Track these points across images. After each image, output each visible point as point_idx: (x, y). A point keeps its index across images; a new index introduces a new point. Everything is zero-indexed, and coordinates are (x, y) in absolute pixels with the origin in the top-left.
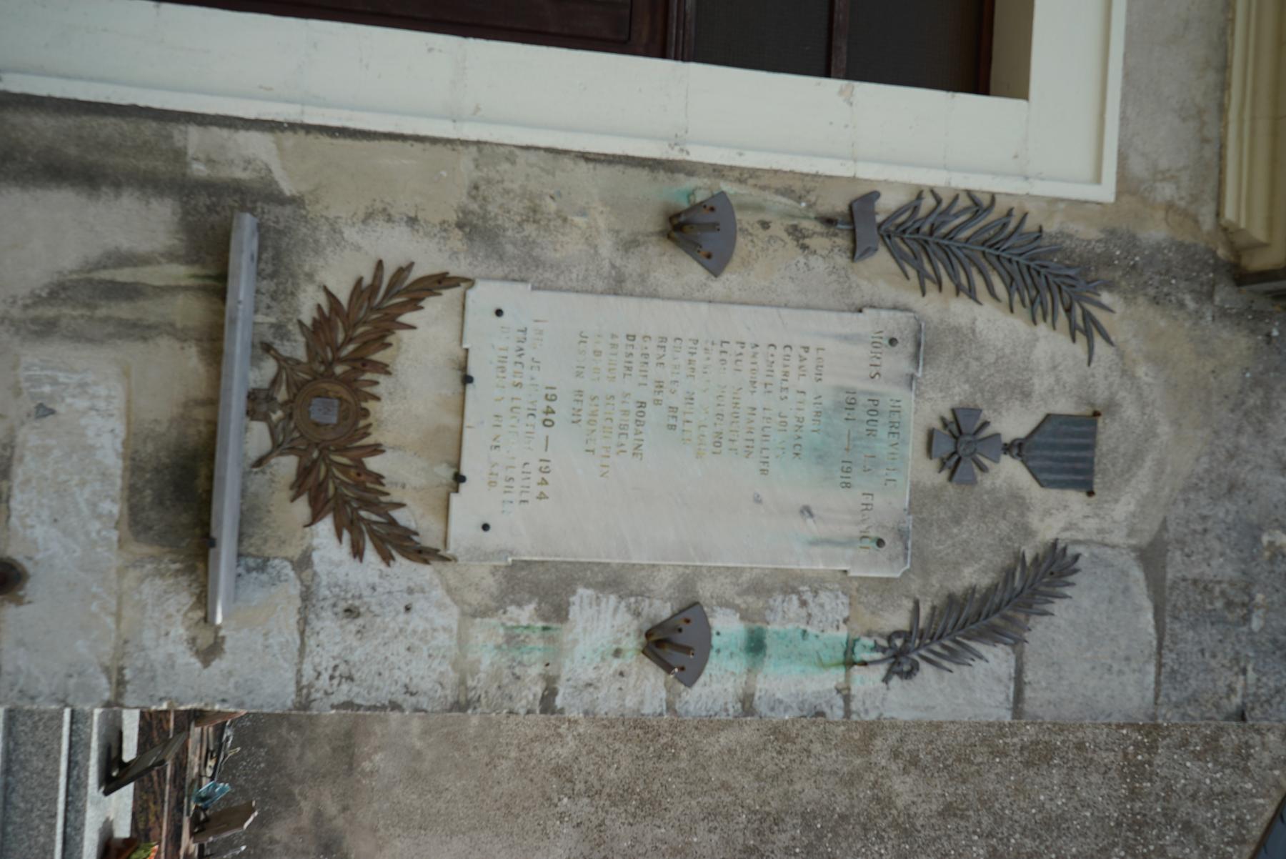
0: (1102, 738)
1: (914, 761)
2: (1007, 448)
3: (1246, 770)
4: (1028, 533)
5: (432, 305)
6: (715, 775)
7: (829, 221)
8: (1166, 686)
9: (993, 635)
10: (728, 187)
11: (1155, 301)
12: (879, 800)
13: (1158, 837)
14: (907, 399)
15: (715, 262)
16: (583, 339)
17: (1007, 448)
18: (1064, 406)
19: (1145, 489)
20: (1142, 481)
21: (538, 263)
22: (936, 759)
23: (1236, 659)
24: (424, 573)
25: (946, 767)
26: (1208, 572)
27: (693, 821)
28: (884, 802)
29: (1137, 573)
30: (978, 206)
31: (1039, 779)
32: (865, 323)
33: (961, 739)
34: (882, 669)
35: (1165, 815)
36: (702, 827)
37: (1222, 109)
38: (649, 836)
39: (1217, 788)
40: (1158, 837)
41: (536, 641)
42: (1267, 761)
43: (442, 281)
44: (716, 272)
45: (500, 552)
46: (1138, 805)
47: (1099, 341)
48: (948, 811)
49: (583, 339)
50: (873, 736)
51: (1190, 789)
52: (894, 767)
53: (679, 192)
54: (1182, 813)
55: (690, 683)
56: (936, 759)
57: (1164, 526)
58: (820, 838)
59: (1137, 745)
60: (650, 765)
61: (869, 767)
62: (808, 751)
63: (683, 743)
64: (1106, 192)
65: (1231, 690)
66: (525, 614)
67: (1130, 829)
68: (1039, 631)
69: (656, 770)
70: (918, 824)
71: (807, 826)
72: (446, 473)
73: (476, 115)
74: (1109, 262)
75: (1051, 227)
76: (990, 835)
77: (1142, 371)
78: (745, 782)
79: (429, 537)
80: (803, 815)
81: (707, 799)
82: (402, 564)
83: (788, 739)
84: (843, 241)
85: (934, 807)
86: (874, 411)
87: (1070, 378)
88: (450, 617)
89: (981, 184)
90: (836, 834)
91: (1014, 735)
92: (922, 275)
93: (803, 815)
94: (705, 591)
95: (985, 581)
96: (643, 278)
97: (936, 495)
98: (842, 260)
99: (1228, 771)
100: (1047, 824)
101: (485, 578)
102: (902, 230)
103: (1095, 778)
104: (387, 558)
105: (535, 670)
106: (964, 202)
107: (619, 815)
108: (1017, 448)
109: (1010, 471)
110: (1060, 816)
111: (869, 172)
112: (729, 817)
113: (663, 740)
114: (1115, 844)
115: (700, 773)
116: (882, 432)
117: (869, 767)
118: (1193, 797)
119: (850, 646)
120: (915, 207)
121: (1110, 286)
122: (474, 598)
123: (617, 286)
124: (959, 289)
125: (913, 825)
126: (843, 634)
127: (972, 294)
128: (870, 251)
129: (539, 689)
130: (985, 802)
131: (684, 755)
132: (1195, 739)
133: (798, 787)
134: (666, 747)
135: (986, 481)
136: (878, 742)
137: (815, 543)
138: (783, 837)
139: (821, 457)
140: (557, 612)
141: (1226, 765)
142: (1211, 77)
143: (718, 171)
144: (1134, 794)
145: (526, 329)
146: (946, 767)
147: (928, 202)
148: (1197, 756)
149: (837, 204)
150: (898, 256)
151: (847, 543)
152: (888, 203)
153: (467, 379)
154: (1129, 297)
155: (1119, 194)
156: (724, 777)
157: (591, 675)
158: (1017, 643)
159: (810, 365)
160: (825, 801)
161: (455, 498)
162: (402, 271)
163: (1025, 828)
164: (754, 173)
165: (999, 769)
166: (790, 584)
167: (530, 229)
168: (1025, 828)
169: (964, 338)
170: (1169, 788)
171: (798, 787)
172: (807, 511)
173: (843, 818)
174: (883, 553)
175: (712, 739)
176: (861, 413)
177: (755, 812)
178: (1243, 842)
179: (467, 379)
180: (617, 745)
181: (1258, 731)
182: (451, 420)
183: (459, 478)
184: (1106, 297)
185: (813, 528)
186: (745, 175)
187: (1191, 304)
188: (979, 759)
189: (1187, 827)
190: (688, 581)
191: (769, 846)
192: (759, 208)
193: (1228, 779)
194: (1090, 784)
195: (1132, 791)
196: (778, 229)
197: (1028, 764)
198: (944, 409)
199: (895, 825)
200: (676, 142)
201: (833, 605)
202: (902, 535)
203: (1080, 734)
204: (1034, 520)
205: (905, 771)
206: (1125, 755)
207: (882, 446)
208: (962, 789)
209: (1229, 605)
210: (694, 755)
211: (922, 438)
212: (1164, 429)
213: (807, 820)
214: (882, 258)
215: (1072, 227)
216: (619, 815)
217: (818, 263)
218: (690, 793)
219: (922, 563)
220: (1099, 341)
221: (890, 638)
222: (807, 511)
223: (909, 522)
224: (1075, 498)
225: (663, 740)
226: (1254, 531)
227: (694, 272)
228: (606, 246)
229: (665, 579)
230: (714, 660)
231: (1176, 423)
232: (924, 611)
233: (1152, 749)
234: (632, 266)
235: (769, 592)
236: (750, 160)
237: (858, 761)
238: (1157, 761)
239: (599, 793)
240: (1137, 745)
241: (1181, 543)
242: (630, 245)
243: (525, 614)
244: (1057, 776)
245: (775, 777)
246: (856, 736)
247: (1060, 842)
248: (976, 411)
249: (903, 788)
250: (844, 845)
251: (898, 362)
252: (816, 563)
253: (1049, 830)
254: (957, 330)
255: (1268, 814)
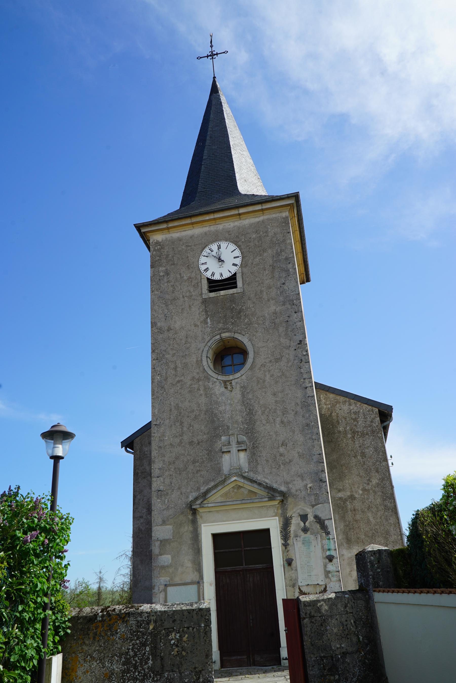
0: (358, 443)
1: (369, 480)
2: (305, 525)
3: (359, 412)
4: (313, 521)
5: (302, 589)
6: (379, 520)
7: (286, 548)
8: (326, 502)
9: (324, 523)
10: (285, 560)
11: (287, 510)
12: (378, 486)
13: (375, 427)
14: (302, 537)
15: (292, 560)
16: (302, 573)
17: (305, 525)
18: (299, 519)
19: (306, 508)
20: (305, 508)
21: (296, 579)
22: (368, 476)
23: (322, 494)
24: (328, 586)
25: (369, 473)
26: (314, 499)
27: (389, 523)
28: (378, 485)
29: (315, 507)
30: (281, 532)
31: (368, 454)
32: (295, 543)
33: (363, 471)
34: (329, 535)
35: (370, 427)
36: (390, 521)
37: (266, 506)
38: (393, 532)
39: (363, 417)
40: (375, 427)
41: (332, 574)
42: (356, 408)
43: (299, 589)
44: (293, 560)
45: (324, 578)
46: (369, 433)
47: (292, 516)
48: (377, 471)
49: (302, 573)
50: (366, 489)
51: (364, 422)
52: (371, 484)
53: (286, 565)
54: (369, 423)
55: (334, 556)
56: (368, 476)
57: (310, 505)
58: (387, 497)
59: (358, 435)
60: (379, 534)
61: (372, 489)
62: (371, 502)
63: (374, 528)
64: (277, 518)
65: (325, 494)
66: (330, 575)
67: (374, 433)
68: (323, 518)
69: (380, 532)
70: (381, 477)
71: (385, 500)
72: (318, 586)
73: (283, 587)
74: (284, 516)
75: (282, 523)
76: (380, 462)
77: (294, 510)
78: (379, 514)
79: (324, 586)
80: (383, 501)
81: (384, 521)
82: (327, 589)
83: (369, 506)
84: (288, 546)
85: (377, 474)
86: (304, 540)
87: (297, 518)
88: (331, 583)
89: (279, 532)
90: (386, 493)
91: (360, 461)
92: (289, 537)
93: (383, 501)
94: (325, 556)
95: (319, 525)
96: (295, 567)
97: (311, 532)
98: (289, 546)
99: (359, 416)
100: (376, 451)
101: (327, 580)
102: (285, 540)
103: (366, 442)
104: (327, 590)
105: (335, 573)
106: (281, 533)
107: (390, 539)
108: (305, 523)
109: (307, 524)
110: (374, 448)
111: (280, 545)
112: (387, 516)
113: (374, 532)
114: (378, 436)
115: (379, 523)
116: (305, 539)
117: (372, 489)
118: (366, 422)
119: (328, 539)
120: (283, 539)
121: (286, 515)
122: (329, 581)
123: (296, 570)
124: (290, 533)
125: (381, 478)
126: (327, 540)
127: (290, 531)
128: (288, 543)
129: (337, 573)
130: (374, 464)
131: (376, 527)
132: (354, 423)
133: (378, 503)
134: (375, 531)
135: (309, 527)
136: (367, 488)
137: (318, 545)
138: (388, 504)
139: (309, 546)
140: (329, 572)
141: (358, 416)
142: (263, 507)
143: (283, 561)
144: (367, 434)
145: (138, 227)
146: (369, 473)
147: (282, 537)
148: (358, 422)
149: (284, 547)
150: (288, 540)
151: (317, 541)
152: (283, 542)
153: (308, 585)
154: (287, 513)
155: (277, 516)
156: (379, 518)
157: (335, 567)
158: (324, 520)
159: (300, 548)
160: (380, 497)
161: (320, 584)
162: (299, 593)
163: (378, 455)
164: (283, 557)
165: (367, 462)
166: (323, 547)
167: (293, 580)
168: (378, 455)
169: (295, 531)
170: (365, 427)
171: (378, 503)
172: (315, 546)
173: (382, 493)
174: (318, 537)
175: (372, 522)
176: (304, 542)
177: (385, 511)
178: (372, 410)
179: (308, 585)
180: (377, 541)
181: (351, 411)
182: (313, 586)
183: (318, 584)
184: (288, 516)
185: (316, 545)
186: (283, 558)
187: (287, 506)
188: (366, 467)
189: (372, 422)
190: (324, 558)
191: (391, 507)
192: (286, 556)
193: (361, 415)
194: (367, 443)
195: (367, 434)
196: (288, 554)
197: (365, 457)
198: (302, 532)
199: (382, 482)
200: (281, 566)
201: (324, 542)
202: (315, 535)
203: (358, 447)
204: (312, 520)
205: (371, 481)
206: (360, 437)
207: (307, 539)
208: (373, 469)
209: (316, 496)
210: (376, 525)
211: (305, 534)
212: (300, 507)
213: (384, 500)
214: (288, 542)
215: (281, 521)
216: (390, 539)
217: (290, 549)
218: (383, 525)
219: (318, 533)
220: (292, 516)
221: (326, 535)
222: (315, 546)
223: (314, 535)
224: (309, 516)
225: (374, 532)
226: (309, 494)
227: (293, 562)
228: (293, 572)
229: (324, 561)
230: (331, 554)
231: (299, 505)
232: (323, 531)
233: (358, 432)
234: (294, 569)
235: (324, 549)
236: (282, 558)
237: (371, 491)
238: (360, 430)
239: (387, 543)
240: (358, 435)
241: (311, 503)
242: (292, 569)
243: (330, 575)
244: (367, 450)
245: (377, 508)
246: (366, 493)
247: (379, 447)
248: (302, 529)
249: (375, 481)
250: (388, 492)
251: (298, 538)
252: (320, 544)
253: (377, 450)
254: (294, 532)
255: (366, 405)
